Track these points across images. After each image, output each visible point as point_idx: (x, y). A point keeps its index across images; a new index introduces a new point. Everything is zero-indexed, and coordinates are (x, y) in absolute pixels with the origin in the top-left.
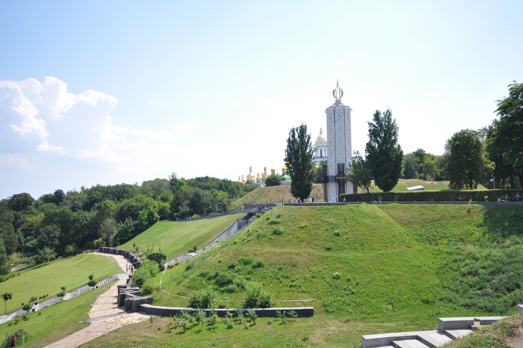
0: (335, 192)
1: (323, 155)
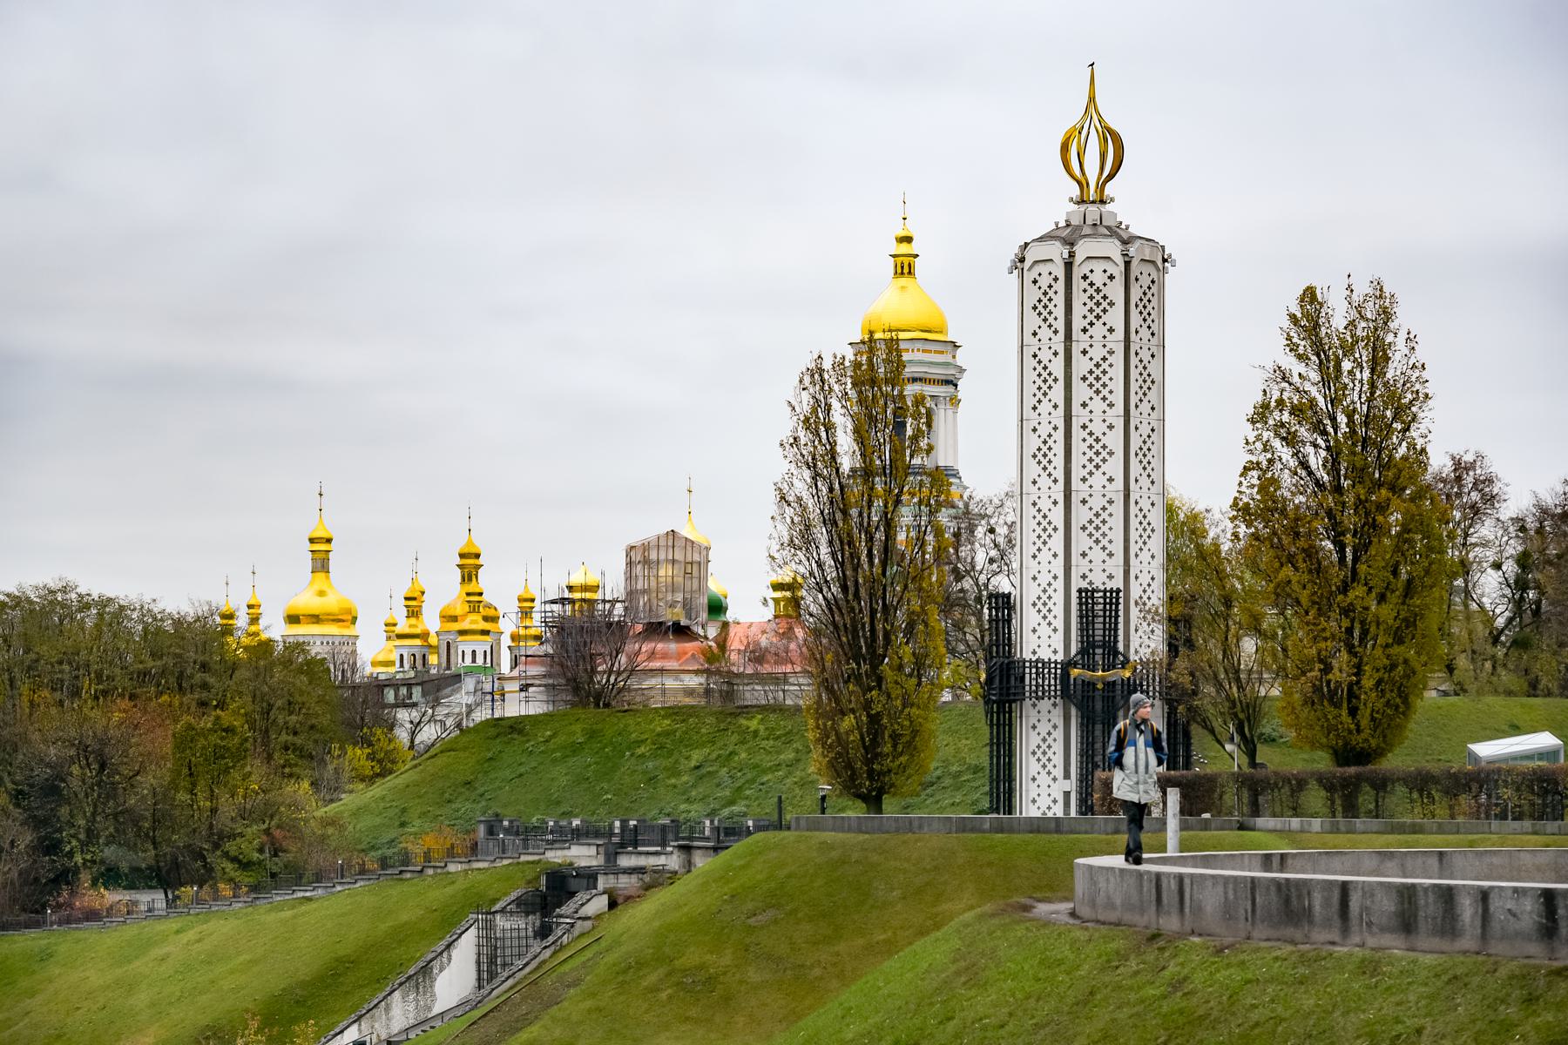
0: (1058, 760)
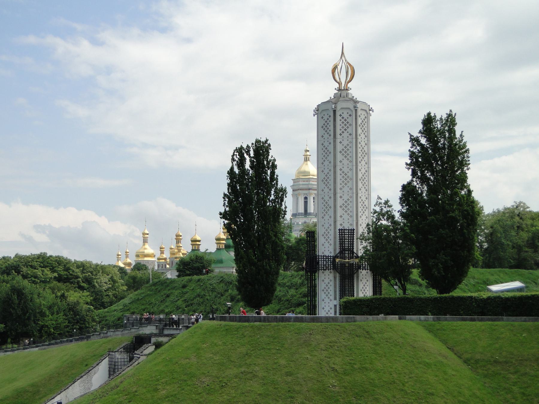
0: (332, 293)
1: (311, 208)
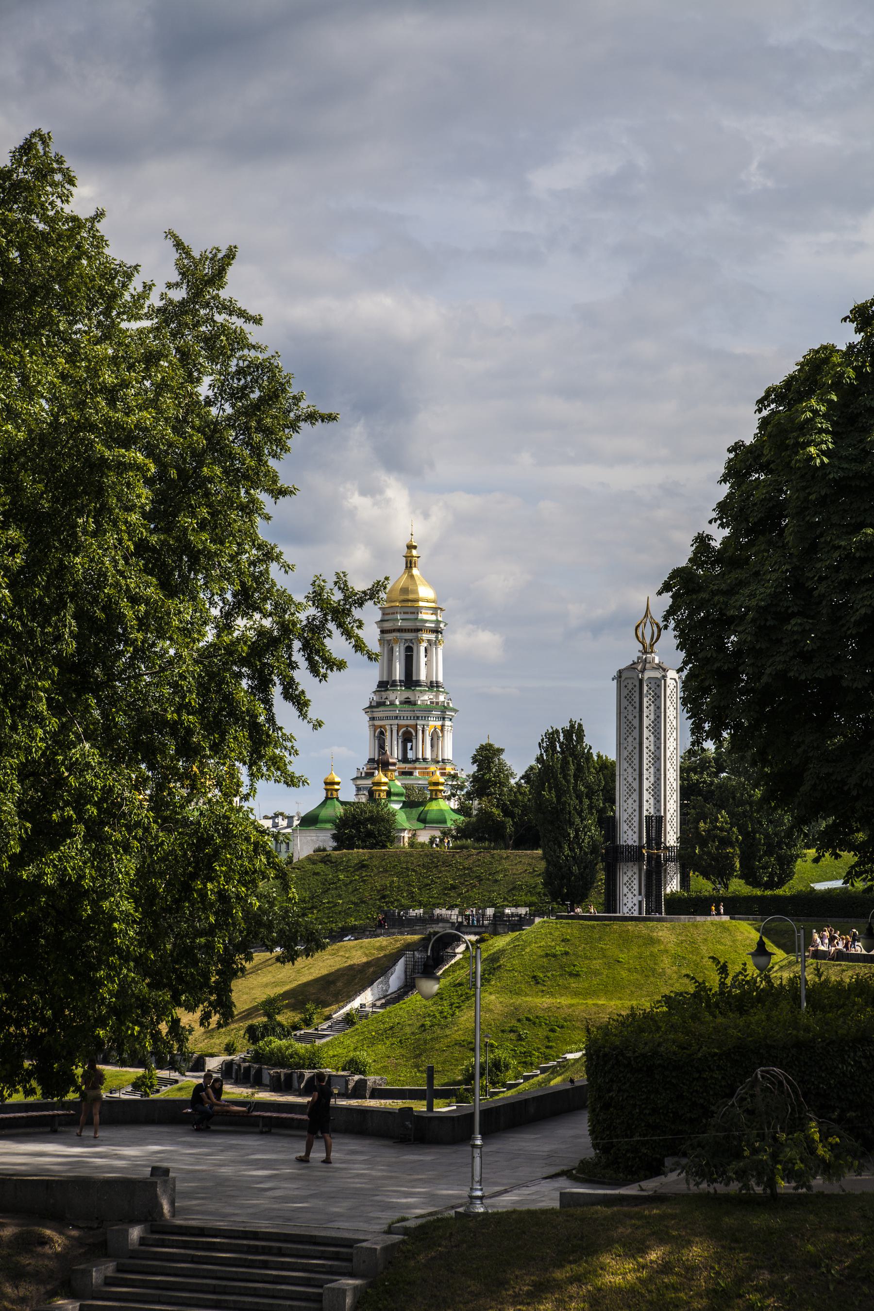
0: (636, 887)
